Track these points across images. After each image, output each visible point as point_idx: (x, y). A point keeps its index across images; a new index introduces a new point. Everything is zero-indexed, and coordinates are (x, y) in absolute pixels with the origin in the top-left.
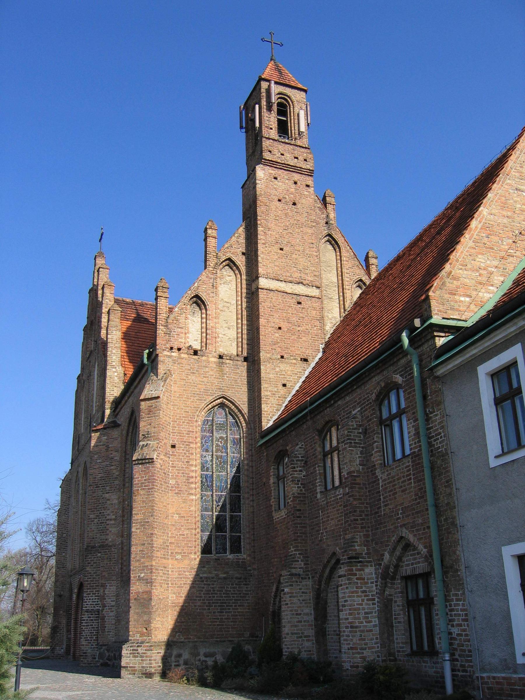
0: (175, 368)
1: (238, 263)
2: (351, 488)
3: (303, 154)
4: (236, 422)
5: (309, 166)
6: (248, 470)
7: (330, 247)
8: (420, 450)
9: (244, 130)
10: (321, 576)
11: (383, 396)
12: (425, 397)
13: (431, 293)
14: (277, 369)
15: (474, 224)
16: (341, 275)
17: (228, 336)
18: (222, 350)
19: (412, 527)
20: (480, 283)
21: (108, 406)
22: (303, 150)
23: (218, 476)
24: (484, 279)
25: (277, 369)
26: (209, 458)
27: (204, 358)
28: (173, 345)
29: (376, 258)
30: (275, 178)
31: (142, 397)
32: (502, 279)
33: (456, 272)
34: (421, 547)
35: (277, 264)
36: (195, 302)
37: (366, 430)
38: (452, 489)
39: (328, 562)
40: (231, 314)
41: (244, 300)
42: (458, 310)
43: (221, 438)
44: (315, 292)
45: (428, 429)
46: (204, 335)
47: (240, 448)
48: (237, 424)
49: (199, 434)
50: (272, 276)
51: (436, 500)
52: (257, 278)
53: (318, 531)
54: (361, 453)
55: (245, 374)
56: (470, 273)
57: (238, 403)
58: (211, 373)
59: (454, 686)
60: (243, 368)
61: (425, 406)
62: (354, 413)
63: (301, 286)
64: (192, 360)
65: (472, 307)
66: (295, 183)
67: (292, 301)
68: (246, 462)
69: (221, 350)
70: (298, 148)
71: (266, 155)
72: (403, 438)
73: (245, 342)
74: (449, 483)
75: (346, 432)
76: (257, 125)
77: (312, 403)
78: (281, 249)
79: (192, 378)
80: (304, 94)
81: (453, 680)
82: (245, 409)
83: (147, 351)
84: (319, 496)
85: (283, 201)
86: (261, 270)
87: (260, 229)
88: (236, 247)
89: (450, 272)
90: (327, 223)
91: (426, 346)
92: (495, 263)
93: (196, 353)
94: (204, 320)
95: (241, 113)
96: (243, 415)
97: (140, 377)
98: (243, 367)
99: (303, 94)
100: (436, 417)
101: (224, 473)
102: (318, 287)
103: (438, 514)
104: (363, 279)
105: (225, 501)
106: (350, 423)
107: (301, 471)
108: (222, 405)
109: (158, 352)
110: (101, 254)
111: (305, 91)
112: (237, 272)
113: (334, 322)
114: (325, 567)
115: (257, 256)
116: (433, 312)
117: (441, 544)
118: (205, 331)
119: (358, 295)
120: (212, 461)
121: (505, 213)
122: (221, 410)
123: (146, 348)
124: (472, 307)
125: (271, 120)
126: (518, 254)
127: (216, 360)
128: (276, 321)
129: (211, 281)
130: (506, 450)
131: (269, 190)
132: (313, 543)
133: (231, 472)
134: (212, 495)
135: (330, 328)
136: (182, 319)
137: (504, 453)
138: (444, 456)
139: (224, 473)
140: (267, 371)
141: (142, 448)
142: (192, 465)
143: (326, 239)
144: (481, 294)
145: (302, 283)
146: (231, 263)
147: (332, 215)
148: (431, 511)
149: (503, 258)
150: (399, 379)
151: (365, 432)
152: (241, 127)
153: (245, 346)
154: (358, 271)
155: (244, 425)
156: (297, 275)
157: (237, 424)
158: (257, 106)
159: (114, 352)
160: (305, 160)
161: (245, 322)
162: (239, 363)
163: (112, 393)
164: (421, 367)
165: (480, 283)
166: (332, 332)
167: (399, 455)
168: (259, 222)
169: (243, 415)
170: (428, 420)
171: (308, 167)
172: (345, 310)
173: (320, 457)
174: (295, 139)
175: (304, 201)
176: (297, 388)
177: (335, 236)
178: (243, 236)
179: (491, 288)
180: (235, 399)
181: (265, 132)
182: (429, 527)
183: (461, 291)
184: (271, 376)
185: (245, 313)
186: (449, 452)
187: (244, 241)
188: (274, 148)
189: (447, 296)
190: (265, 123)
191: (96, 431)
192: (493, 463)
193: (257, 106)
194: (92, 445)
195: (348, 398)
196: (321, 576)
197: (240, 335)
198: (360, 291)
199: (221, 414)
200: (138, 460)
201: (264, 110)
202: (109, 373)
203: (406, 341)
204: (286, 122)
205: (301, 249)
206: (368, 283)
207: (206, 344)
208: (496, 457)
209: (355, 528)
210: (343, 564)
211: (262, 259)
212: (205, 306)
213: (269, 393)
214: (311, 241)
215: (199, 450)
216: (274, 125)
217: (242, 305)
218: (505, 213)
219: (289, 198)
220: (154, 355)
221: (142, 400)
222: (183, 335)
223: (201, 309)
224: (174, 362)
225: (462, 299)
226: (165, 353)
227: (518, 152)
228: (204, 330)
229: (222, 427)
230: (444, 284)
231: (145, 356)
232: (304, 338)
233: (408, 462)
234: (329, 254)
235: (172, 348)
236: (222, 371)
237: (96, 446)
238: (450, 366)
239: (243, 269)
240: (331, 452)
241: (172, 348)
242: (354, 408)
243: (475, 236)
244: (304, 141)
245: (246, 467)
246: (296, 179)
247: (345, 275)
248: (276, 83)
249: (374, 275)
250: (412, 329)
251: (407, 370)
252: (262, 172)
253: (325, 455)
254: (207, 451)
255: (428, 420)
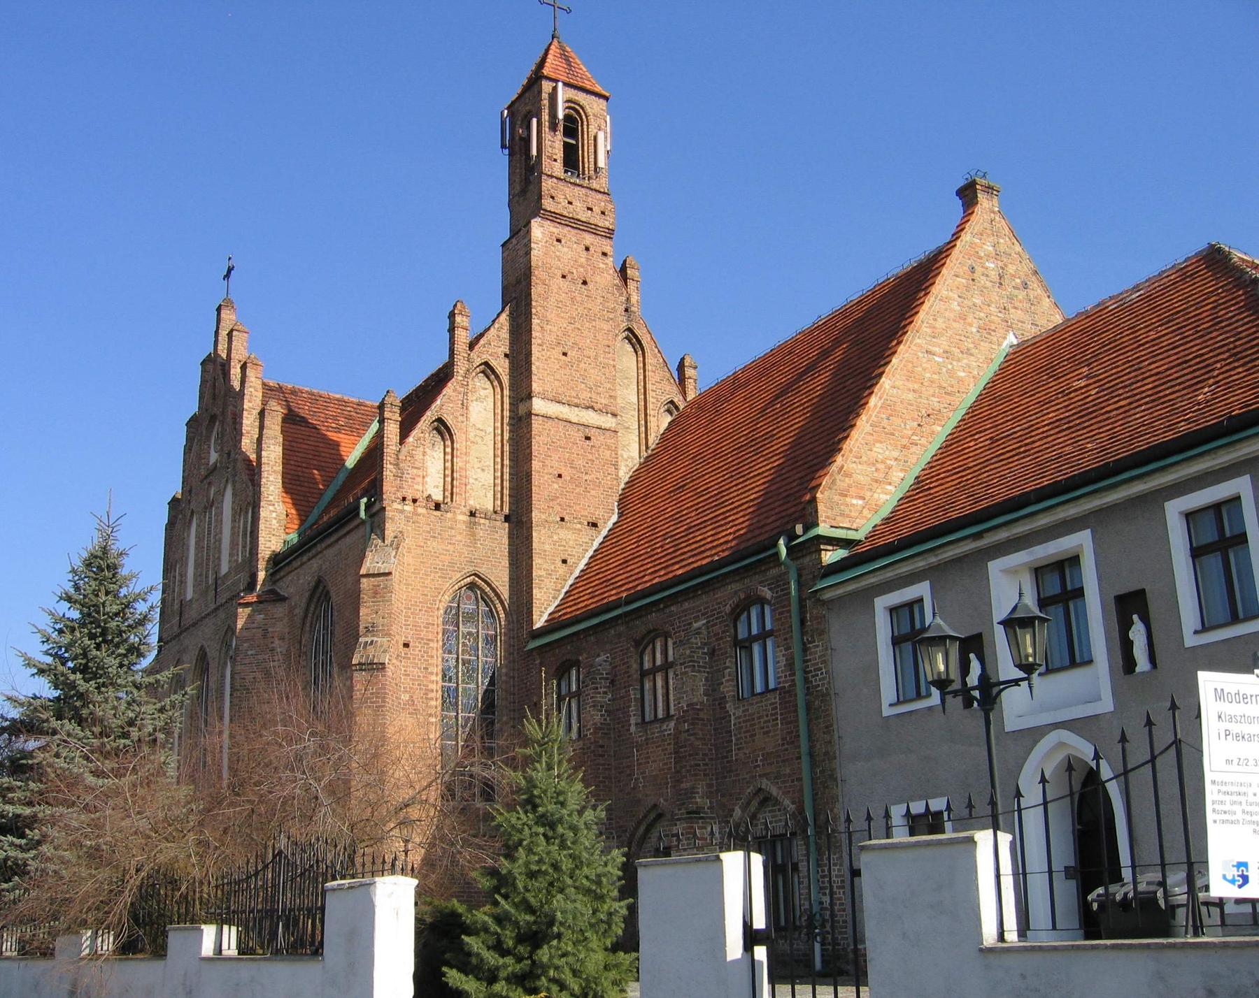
0: (409, 529)
1: (499, 370)
2: (693, 724)
3: (599, 202)
4: (491, 610)
5: (607, 223)
6: (506, 682)
7: (629, 348)
8: (794, 685)
9: (506, 152)
10: (633, 835)
11: (741, 608)
12: (803, 622)
13: (819, 495)
14: (555, 538)
15: (873, 401)
16: (644, 393)
17: (483, 483)
18: (473, 503)
19: (776, 778)
20: (876, 481)
21: (262, 565)
22: (600, 196)
23: (465, 689)
24: (881, 476)
25: (555, 538)
26: (452, 663)
27: (449, 515)
28: (405, 494)
29: (695, 368)
30: (559, 241)
31: (363, 571)
32: (902, 475)
33: (850, 466)
34: (787, 802)
35: (558, 377)
36: (437, 429)
37: (714, 650)
38: (832, 736)
39: (645, 817)
40: (485, 448)
41: (506, 428)
42: (848, 516)
43: (470, 634)
44: (608, 421)
45: (805, 661)
46: (449, 479)
47: (495, 649)
48: (491, 614)
49: (441, 627)
50: (550, 396)
51: (811, 747)
52: (530, 397)
53: (629, 775)
54: (707, 679)
55: (506, 541)
56: (865, 467)
57: (496, 584)
58: (459, 537)
59: (823, 961)
60: (502, 533)
61: (803, 634)
62: (696, 625)
63: (590, 412)
64: (432, 518)
65: (866, 512)
66: (587, 249)
67: (578, 436)
68: (504, 670)
69: (471, 502)
70: (593, 193)
71: (547, 204)
72: (768, 666)
73: (506, 492)
74: (828, 729)
75: (688, 652)
76: (534, 152)
77: (629, 601)
78: (565, 354)
79: (433, 544)
80: (604, 102)
81: (822, 955)
82: (505, 594)
83: (365, 500)
84: (633, 729)
85: (569, 277)
86: (536, 387)
87: (535, 321)
88: (496, 347)
89: (842, 467)
90: (626, 310)
91: (807, 559)
92: (895, 454)
93: (438, 507)
94: (449, 457)
95: (503, 123)
96: (502, 602)
97: (341, 533)
98: (503, 531)
99: (602, 102)
100: (817, 649)
101: (472, 686)
102: (614, 415)
103: (813, 764)
104: (676, 400)
105: (473, 724)
106: (693, 640)
107: (605, 693)
108: (472, 586)
109: (385, 503)
110: (228, 303)
111: (607, 98)
112: (496, 383)
113: (630, 465)
114: (639, 823)
115: (529, 363)
116: (821, 519)
117: (814, 800)
118: (451, 476)
119: (665, 425)
120: (457, 667)
121: (910, 385)
122: (470, 593)
123: (362, 497)
124: (866, 512)
125: (554, 145)
126: (923, 441)
127: (466, 518)
128: (555, 464)
129: (461, 397)
130: (901, 699)
131: (549, 260)
132: (621, 791)
133: (483, 683)
134: (457, 718)
135: (624, 474)
136: (419, 456)
137: (899, 702)
138: (825, 697)
139: (472, 686)
140: (541, 539)
141: (365, 647)
142: (432, 673)
143: (624, 335)
144: (876, 496)
145: (592, 408)
146: (488, 370)
147: (634, 298)
148: (805, 760)
149: (904, 447)
150: (767, 593)
151: (712, 653)
152: (503, 146)
153: (506, 499)
154: (668, 388)
155: (502, 615)
156: (585, 395)
157: (491, 614)
158: (535, 120)
159: (271, 478)
160: (603, 213)
161: (507, 462)
162: (498, 523)
163: (268, 544)
164: (800, 586)
165: (876, 481)
166: (627, 479)
167: (759, 688)
168: (534, 311)
169: (502, 602)
170: (805, 650)
171: (607, 224)
172: (647, 448)
173: (637, 676)
174: (589, 178)
175: (598, 278)
176: (582, 566)
177: (637, 332)
178: (506, 327)
179: (889, 487)
180: (492, 578)
181: (546, 166)
182: (800, 779)
183: (853, 491)
184: (547, 547)
185: (507, 448)
186: (832, 692)
187: (507, 336)
188: (558, 192)
189: (836, 498)
190: (547, 150)
191: (247, 605)
192: (887, 711)
193: (535, 120)
194: (239, 626)
195: (686, 605)
196: (633, 835)
197: (499, 481)
198: (669, 419)
199: (469, 598)
200: (360, 664)
201: (546, 129)
202: (263, 513)
203: (783, 551)
204: (575, 147)
205: (592, 354)
206: (681, 407)
207: (452, 494)
208: (891, 705)
209: (696, 775)
210: (679, 819)
211: (538, 368)
212: (451, 435)
213: (543, 573)
214: (607, 342)
215: (440, 651)
216: (559, 155)
217: (502, 435)
218: (910, 385)
219: (578, 273)
220: (377, 507)
221: (364, 576)
222: (420, 480)
223: (443, 439)
224: (408, 519)
225: (854, 501)
226: (396, 506)
227: (932, 299)
228: (448, 472)
229: (471, 618)
230: (834, 482)
231: (363, 507)
232: (593, 492)
233: (775, 698)
234: (627, 359)
235: (404, 499)
236: (473, 535)
237: (244, 628)
238: (840, 591)
239: (505, 379)
240: (654, 671)
241: (404, 499)
242: (697, 619)
243: (873, 418)
244: (602, 183)
245: (504, 678)
246: (588, 243)
247: (650, 394)
248: (566, 84)
249: (691, 396)
250: (792, 536)
251: (780, 584)
252: (539, 230)
253: (643, 674)
254: (450, 652)
255: (805, 650)
